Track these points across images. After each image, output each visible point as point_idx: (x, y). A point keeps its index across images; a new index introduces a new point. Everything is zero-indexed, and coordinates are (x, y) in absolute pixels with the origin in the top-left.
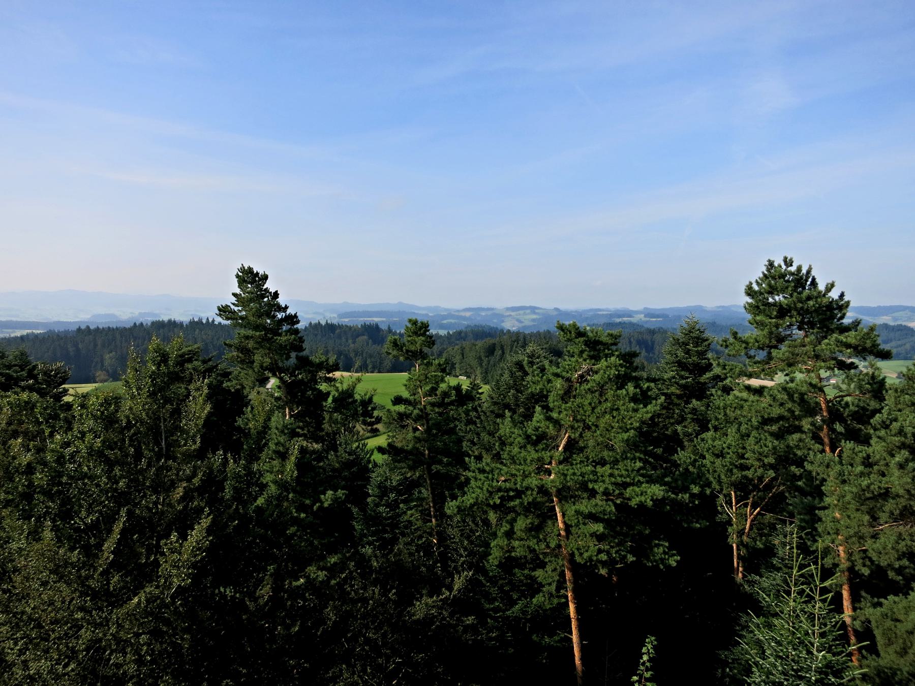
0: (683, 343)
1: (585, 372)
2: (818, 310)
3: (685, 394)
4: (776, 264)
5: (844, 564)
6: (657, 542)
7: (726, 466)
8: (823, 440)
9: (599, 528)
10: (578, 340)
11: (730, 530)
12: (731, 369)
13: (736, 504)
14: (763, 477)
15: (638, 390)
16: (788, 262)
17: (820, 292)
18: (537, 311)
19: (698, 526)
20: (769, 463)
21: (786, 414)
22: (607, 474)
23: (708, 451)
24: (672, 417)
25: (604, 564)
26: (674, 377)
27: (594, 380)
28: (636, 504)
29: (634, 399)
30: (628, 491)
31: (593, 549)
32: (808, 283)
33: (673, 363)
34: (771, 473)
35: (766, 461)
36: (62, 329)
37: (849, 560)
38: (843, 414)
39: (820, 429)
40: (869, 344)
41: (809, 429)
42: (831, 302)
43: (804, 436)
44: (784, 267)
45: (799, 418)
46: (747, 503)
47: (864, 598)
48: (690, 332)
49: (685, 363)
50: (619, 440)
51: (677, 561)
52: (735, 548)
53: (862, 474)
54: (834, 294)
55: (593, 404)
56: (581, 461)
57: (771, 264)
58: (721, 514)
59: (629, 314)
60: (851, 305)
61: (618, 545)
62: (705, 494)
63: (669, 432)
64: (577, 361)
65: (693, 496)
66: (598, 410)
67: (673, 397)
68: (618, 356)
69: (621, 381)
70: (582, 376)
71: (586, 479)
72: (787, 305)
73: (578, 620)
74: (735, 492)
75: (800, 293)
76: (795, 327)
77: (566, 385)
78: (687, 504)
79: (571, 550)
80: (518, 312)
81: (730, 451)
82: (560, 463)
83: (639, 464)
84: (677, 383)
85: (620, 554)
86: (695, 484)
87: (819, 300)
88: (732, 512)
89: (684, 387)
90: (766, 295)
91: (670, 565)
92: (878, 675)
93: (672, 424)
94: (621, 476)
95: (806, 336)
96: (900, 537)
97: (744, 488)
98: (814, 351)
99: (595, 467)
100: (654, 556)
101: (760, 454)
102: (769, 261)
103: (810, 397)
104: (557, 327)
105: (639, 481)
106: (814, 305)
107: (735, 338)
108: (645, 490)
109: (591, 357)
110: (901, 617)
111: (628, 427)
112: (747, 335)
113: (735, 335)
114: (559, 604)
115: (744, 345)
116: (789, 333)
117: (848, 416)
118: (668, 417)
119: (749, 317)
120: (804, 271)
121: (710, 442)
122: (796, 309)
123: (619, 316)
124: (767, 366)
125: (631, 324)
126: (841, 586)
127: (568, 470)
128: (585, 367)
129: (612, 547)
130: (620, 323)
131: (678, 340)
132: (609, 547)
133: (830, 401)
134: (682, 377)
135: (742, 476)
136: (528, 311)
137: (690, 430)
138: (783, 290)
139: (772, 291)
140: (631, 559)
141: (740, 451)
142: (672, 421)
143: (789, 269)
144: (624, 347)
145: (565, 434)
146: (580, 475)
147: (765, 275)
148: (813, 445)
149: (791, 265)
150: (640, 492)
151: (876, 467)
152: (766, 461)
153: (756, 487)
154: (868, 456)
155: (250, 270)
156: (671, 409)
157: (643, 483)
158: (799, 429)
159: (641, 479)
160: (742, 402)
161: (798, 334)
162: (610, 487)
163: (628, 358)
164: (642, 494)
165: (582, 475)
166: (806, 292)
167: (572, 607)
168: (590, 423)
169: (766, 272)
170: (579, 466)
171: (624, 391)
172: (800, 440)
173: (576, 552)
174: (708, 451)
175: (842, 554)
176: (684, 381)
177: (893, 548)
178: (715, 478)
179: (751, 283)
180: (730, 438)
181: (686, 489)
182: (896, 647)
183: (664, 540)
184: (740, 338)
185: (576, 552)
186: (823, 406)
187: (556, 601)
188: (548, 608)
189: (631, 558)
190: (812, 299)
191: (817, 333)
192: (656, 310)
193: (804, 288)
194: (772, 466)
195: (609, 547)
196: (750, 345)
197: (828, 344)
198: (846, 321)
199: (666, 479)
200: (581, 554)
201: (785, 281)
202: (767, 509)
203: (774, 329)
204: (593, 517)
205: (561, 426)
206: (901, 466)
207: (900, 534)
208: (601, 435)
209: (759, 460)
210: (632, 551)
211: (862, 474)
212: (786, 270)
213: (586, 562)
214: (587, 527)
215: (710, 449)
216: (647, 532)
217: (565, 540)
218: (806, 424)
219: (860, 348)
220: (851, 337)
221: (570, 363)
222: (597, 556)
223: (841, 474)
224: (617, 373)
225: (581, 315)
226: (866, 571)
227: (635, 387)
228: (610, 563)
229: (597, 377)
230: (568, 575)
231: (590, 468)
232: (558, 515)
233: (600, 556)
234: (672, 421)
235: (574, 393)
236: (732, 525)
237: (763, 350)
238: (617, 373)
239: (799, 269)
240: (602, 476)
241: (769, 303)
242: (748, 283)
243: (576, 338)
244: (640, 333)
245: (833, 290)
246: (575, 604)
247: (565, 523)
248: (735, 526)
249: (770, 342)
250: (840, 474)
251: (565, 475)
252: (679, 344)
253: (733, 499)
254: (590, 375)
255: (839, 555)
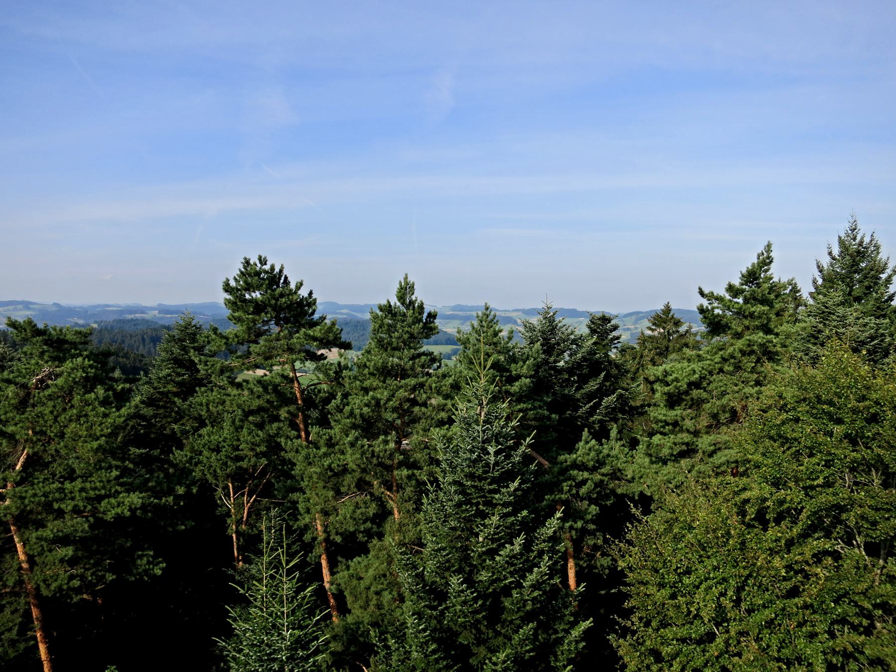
0: (179, 340)
1: (46, 376)
2: (290, 307)
3: (182, 391)
4: (252, 262)
5: (321, 536)
6: (140, 553)
7: (221, 460)
8: (299, 426)
9: (68, 551)
10: (35, 339)
11: (229, 521)
12: (213, 365)
13: (234, 495)
14: (256, 465)
15: (111, 393)
16: (263, 261)
17: (291, 290)
18: (31, 306)
19: (183, 527)
20: (261, 452)
21: (265, 405)
22: (76, 489)
23: (204, 447)
24: (170, 416)
25: (78, 591)
26: (169, 375)
27: (56, 385)
28: (113, 517)
29: (105, 403)
30: (102, 504)
31: (63, 576)
32: (282, 281)
33: (169, 360)
34: (264, 461)
35: (258, 450)
36: (111, 318)
37: (325, 531)
38: (315, 401)
39: (296, 416)
40: (331, 337)
41: (285, 418)
42: (302, 300)
43: (281, 425)
44: (259, 265)
45: (278, 408)
46: (244, 492)
47: (341, 562)
48: (186, 328)
49: (180, 360)
50: (86, 449)
51: (163, 569)
52: (234, 538)
53: (325, 455)
54: (303, 292)
55: (55, 413)
56: (45, 479)
57: (247, 262)
58: (221, 507)
59: (143, 310)
60: (318, 301)
61: (95, 565)
62: (192, 493)
63: (167, 432)
64: (37, 363)
65: (178, 498)
66: (62, 418)
67: (170, 395)
68: (87, 356)
69: (89, 384)
70: (42, 381)
71: (50, 499)
72: (262, 301)
73: (51, 661)
74: (233, 484)
75: (274, 290)
76: (273, 322)
77: (22, 393)
78: (173, 506)
79: (36, 583)
80: (6, 308)
81: (225, 444)
82: (18, 484)
83: (115, 473)
84: (174, 381)
85: (97, 576)
86: (181, 485)
87: (290, 297)
88: (230, 504)
89: (179, 384)
90: (244, 292)
91: (155, 575)
92: (346, 632)
93: (170, 423)
94: (95, 489)
95: (281, 331)
96: (357, 506)
97: (240, 478)
98: (287, 345)
99: (62, 483)
100: (137, 569)
101: (253, 444)
102: (245, 259)
103: (284, 387)
104: (8, 325)
105: (116, 491)
106: (285, 303)
107: (215, 333)
108: (122, 500)
109: (53, 359)
110: (362, 575)
111: (98, 434)
112: (228, 331)
113: (215, 330)
114: (26, 648)
115: (224, 341)
116: (266, 328)
117: (319, 402)
118: (165, 417)
119: (228, 312)
120: (277, 270)
121: (206, 437)
122: (271, 306)
123: (131, 312)
124: (246, 361)
125: (143, 320)
126: (320, 556)
127: (26, 491)
128: (46, 369)
129: (88, 569)
130: (132, 320)
131: (174, 336)
132: (82, 570)
133: (304, 390)
134: (179, 375)
135: (236, 467)
136: (20, 306)
137: (187, 428)
138: (258, 288)
139: (249, 288)
140: (111, 578)
141: (235, 443)
142: (169, 420)
143: (264, 267)
144: (94, 346)
145: (23, 450)
146: (43, 495)
147: (242, 272)
148: (290, 432)
149: (265, 264)
150: (116, 504)
151: (337, 447)
152: (258, 450)
153: (252, 476)
154: (331, 438)
155: (274, 279)
156: (167, 408)
157: (121, 493)
158: (277, 419)
159: (119, 488)
160: (224, 397)
161: (275, 329)
162: (81, 504)
163: (101, 358)
164: (118, 506)
165: (45, 495)
166: (279, 290)
167: (42, 648)
168: (52, 434)
169: (243, 270)
170: (41, 484)
171: (93, 395)
172: (279, 428)
173: (42, 584)
174: (204, 447)
175: (319, 527)
176: (181, 378)
177: (351, 517)
178: (211, 473)
179: (228, 280)
180: (226, 432)
181: (171, 491)
182: (361, 602)
183: (149, 549)
184: (220, 334)
185: (42, 584)
186: (298, 395)
187: (22, 646)
188: (13, 655)
189: (110, 577)
190: (284, 296)
191: (290, 327)
192: (172, 306)
193: (278, 286)
194: (264, 454)
195: (82, 570)
196: (230, 340)
197: (298, 339)
198: (316, 316)
199: (150, 484)
200: (48, 586)
201: (261, 279)
202: (262, 495)
203: (251, 325)
204: (64, 540)
205: (17, 441)
206: (352, 445)
207: (357, 503)
208: (65, 447)
209: (252, 450)
210: (111, 570)
211: (325, 455)
212: (260, 268)
213: (55, 594)
214: (54, 553)
215: (206, 444)
216: (128, 545)
217: (29, 573)
218: (283, 413)
219: (324, 341)
220: (317, 332)
221: (28, 366)
222: (67, 583)
223: (307, 457)
224: (84, 375)
225: (87, 312)
226: (338, 539)
227: (106, 390)
228: (87, 587)
229: (60, 381)
230: (35, 612)
231: (56, 485)
232: (18, 545)
233: (71, 584)
234: (169, 420)
235: (32, 401)
236: (231, 516)
237: (243, 345)
238: (84, 375)
239: (273, 268)
240: (71, 492)
241: (246, 300)
242: (225, 280)
243: (33, 336)
244: (155, 330)
245: (302, 288)
246: (46, 643)
247: (25, 553)
248: (233, 516)
249: (250, 337)
250: (306, 458)
251: (22, 498)
252: (174, 340)
253: (231, 490)
254: (51, 379)
255: (317, 529)
